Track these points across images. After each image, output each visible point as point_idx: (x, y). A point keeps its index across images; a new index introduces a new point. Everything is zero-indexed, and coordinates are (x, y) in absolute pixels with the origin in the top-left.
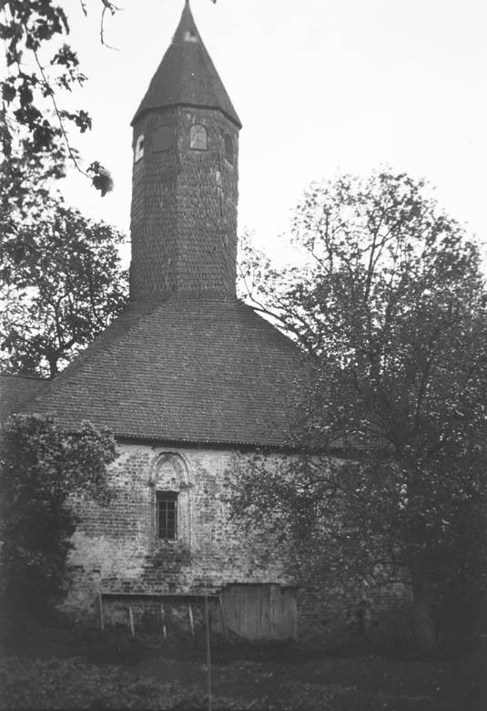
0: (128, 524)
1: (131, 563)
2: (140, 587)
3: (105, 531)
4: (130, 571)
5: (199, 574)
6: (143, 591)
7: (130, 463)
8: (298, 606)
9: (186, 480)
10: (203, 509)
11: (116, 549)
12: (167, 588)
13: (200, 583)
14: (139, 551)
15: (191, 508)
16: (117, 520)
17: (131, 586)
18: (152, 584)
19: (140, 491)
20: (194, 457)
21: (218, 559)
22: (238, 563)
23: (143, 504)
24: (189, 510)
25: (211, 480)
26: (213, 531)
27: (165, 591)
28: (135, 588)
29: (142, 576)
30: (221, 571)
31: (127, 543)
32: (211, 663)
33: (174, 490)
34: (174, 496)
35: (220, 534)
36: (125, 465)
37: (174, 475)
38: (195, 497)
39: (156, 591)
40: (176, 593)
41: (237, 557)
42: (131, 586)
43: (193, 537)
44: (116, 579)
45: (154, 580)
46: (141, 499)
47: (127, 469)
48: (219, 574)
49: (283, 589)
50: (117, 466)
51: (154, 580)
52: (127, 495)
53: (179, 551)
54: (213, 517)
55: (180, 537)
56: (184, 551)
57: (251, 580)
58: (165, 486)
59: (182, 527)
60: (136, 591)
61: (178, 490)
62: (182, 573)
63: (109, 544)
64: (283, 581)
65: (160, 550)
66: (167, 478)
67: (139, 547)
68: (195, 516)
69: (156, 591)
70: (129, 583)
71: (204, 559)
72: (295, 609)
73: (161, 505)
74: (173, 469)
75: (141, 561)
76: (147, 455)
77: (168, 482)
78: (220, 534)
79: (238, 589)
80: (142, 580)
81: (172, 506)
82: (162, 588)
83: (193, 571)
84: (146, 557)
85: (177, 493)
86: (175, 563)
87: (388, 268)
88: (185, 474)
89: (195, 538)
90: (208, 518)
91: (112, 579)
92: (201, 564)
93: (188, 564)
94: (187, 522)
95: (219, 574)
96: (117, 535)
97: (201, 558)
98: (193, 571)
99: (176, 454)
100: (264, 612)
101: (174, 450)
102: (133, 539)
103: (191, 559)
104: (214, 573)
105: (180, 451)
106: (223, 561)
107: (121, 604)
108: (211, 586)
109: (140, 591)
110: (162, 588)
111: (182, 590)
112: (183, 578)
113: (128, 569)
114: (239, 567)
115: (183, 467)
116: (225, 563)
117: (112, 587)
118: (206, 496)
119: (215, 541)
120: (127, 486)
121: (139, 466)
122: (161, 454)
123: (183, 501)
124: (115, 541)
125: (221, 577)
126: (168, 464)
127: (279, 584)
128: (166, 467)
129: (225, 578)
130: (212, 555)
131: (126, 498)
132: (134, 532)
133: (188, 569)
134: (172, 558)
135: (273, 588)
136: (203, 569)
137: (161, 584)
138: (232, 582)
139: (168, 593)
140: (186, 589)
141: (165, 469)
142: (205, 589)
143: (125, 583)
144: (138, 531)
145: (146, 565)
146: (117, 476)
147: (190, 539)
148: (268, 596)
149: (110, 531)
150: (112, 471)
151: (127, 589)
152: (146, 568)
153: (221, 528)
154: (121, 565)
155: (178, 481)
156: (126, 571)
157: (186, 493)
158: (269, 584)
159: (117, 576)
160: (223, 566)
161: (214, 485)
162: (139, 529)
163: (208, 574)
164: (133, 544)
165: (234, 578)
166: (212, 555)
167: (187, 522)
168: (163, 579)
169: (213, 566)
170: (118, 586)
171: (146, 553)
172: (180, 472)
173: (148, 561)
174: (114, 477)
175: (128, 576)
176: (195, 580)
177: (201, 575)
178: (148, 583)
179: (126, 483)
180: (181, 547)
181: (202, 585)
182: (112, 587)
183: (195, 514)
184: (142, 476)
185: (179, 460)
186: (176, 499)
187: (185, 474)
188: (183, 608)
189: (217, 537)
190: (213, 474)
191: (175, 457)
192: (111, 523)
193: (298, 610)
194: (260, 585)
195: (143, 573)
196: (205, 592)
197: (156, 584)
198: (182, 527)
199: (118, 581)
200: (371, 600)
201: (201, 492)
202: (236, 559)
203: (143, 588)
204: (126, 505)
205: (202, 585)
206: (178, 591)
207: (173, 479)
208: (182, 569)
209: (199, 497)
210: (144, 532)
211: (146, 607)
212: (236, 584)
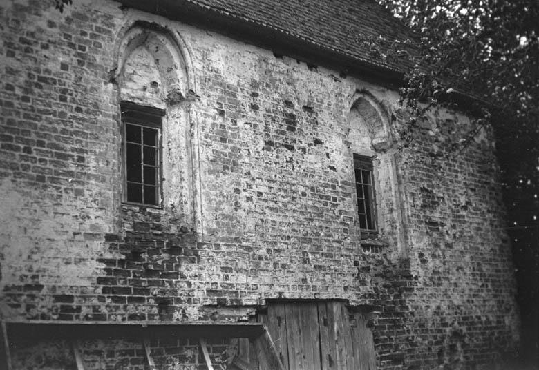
0: (66, 157)
1: (75, 250)
2: (95, 308)
3: (13, 166)
4: (72, 267)
5: (215, 279)
6: (102, 317)
7: (74, 26)
8: (376, 341)
9: (182, 87)
10: (217, 146)
11: (40, 213)
12: (155, 310)
13: (221, 301)
14: (93, 221)
15: (195, 141)
16: (41, 144)
17: (74, 305)
18: (122, 300)
19: (93, 89)
20: (198, 44)
21: (249, 249)
22: (283, 259)
23: (100, 118)
24: (190, 145)
25: (230, 92)
26: (237, 191)
27: (151, 317)
28: (85, 310)
29: (100, 280)
30: (255, 272)
31: (66, 200)
32: (199, 360)
33: (156, 105)
34: (154, 117)
35: (249, 199)
36: (61, 27)
37: (156, 77)
38: (201, 119)
39: (132, 317)
40: (174, 322)
41: (279, 246)
42: (74, 305)
43: (201, 201)
44: (40, 287)
45: (127, 291)
46: (96, 106)
47: (67, 36)
48: (251, 281)
49: (352, 310)
50: (44, 25)
51: (127, 291)
52: (64, 91)
53: (174, 230)
54: (235, 164)
55: (171, 201)
56: (183, 230)
57: (306, 294)
58: (140, 93)
59: (174, 180)
60: (86, 317)
61: (163, 106)
62: (184, 277)
63: (23, 201)
64: (354, 299)
65: (134, 226)
66: (142, 79)
67: (93, 213)
68: (203, 157)
69: (132, 317)
70: (70, 298)
71: (223, 249)
72: (371, 345)
73: (131, 134)
74: (152, 64)
75: (99, 245)
76: (111, 17)
77: (145, 89)
78: (249, 199)
79: (280, 311)
80: (99, 290)
81: (151, 137)
82: (143, 309)
83: (204, 273)
84: (109, 237)
85: (163, 113)
86: (165, 256)
87: (28, 254)
88: (180, 74)
89: (204, 203)
90: (227, 163)
91: (28, 287)
92: (219, 258)
93: (194, 257)
94: (185, 170)
95: (251, 281)
96: (41, 179)
97: (218, 246)
98: (204, 273)
99: (166, 32)
100: (325, 354)
101: (163, 22)
102: (79, 193)
103: (200, 245)
104: (242, 279)
105: (174, 27)
106: (258, 253)
107: (51, 352)
108: (240, 306)
109: (96, 317)
110: (143, 309)
111: (184, 316)
112: (186, 287)
113: (67, 263)
114: (283, 266)
115: (177, 61)
116: (260, 258)
117: (29, 308)
118: (220, 120)
119: (240, 212)
120: (65, 74)
121: (93, 36)
122: (138, 24)
123: (174, 128)
124: (37, 193)
125: (255, 286)
126: (144, 52)
127: (347, 301)
128: (141, 58)
129: (263, 289)
130: (236, 239)
131: (63, 99)
132: (81, 178)
133: (195, 269)
134: (160, 243)
135: (336, 309)
136: (224, 269)
137: (141, 300)
138: (275, 296)
139: (156, 322)
140: (194, 313)
141: (137, 60)
142: (225, 313)
143: (58, 298)
144: (89, 176)
145: (109, 256)
146: (45, 47)
147: (193, 204)
148: (328, 323)
149: (26, 168)
150: (32, 34)
151: (66, 312)
152: (110, 262)
153: (249, 186)
154: (52, 253)
155: (164, 90)
156: (63, 268)
157: (182, 112)
158: (332, 300)
159: (42, 281)
160: (257, 265)
161: (235, 104)
162: (93, 172)
163: (232, 280)
164: (79, 203)
165: (279, 289)
166: (236, 239)
167: (185, 170)
168: (147, 291)
169: (241, 264)
170: (44, 303)
171: (107, 228)
172: (170, 69)
173: (113, 247)
174: (38, 48)
175: (68, 282)
176: (210, 292)
177: (220, 281)
178: (115, 300)
179: (64, 67)
180: (175, 221)
181: (221, 304)
182: (29, 308)
183: (204, 154)
184: (98, 58)
185: (169, 46)
186: (160, 124)
187: (180, 74)
188: (189, 353)
189: (244, 204)
190: (232, 81)
191: (161, 38)
192: (28, 150)
193: (376, 347)
194: (317, 302)
195: (103, 275)
196: (227, 317)
197: (131, 300)
198: (174, 180)
199: (44, 291)
200: (464, 329)
201: (213, 112)
202: (278, 251)
203: (104, 310)
204: (62, 114)
205: (221, 304)
206: (177, 315)
207: (154, 84)
208: (183, 268)
209: (209, 121)
210: (103, 180)
211: (111, 354)
212: (280, 301)
